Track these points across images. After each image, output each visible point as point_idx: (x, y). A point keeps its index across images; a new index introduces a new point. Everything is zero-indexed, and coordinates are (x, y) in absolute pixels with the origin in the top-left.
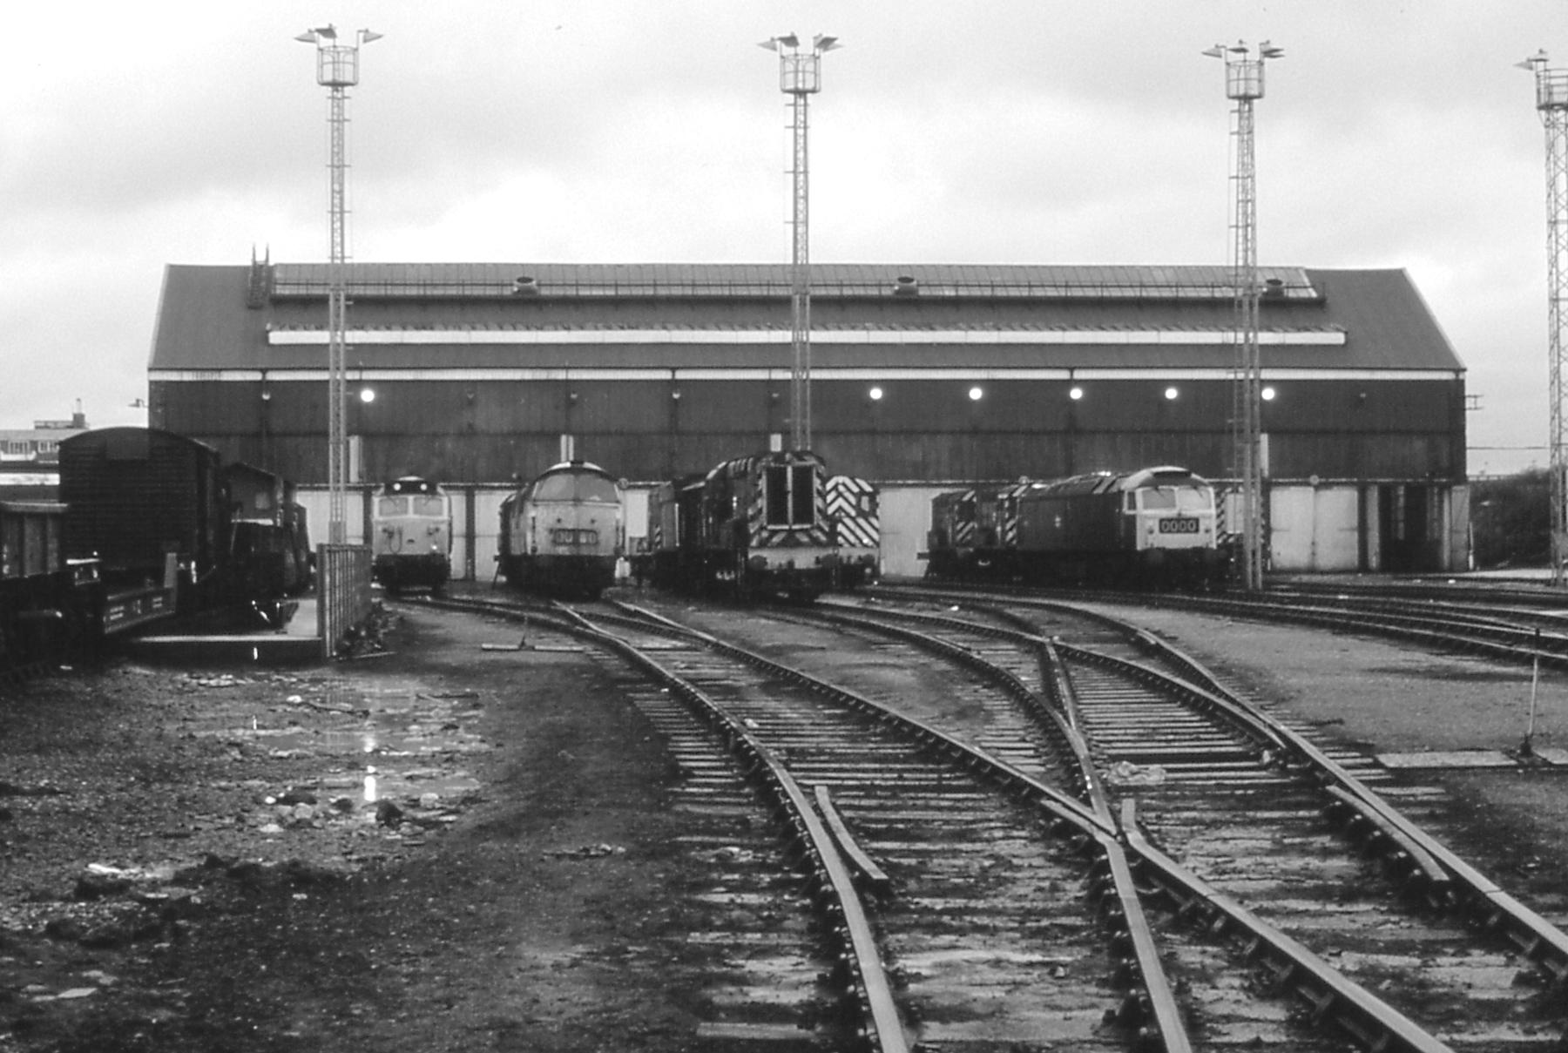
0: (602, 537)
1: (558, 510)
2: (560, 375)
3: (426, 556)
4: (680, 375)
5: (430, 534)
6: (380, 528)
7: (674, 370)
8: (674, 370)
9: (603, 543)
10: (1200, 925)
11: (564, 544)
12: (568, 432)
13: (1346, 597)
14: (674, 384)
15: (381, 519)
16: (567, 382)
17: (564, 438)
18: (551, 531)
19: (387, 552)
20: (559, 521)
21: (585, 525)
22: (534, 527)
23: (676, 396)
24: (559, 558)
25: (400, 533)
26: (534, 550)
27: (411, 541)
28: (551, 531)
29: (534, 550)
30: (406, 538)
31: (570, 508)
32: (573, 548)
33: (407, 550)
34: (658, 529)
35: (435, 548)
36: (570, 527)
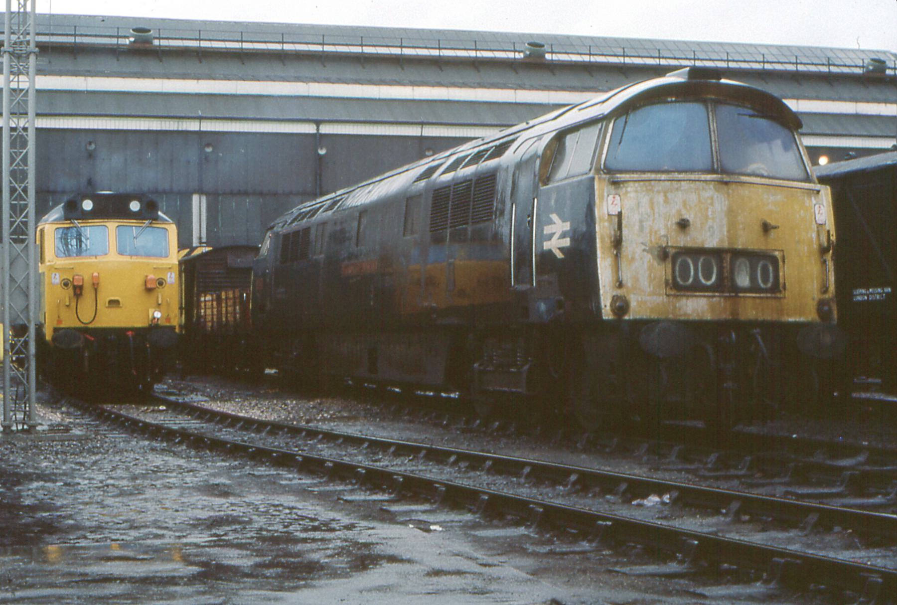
0: (787, 272)
1: (678, 198)
2: (193, 126)
3: (138, 331)
4: (325, 129)
5: (149, 290)
6: (57, 279)
7: (318, 123)
8: (318, 123)
9: (791, 294)
10: (153, 591)
11: (697, 288)
12: (201, 192)
13: (690, 423)
14: (319, 139)
15: (62, 262)
16: (200, 134)
17: (195, 198)
18: (663, 254)
19: (69, 322)
20: (683, 225)
21: (748, 239)
22: (618, 243)
23: (322, 152)
24: (696, 327)
25: (96, 287)
26: (621, 308)
27: (114, 303)
28: (663, 254)
29: (621, 308)
30: (105, 296)
31: (710, 192)
32: (717, 299)
33: (109, 319)
34: (743, 280)
35: (158, 315)
36: (712, 243)
